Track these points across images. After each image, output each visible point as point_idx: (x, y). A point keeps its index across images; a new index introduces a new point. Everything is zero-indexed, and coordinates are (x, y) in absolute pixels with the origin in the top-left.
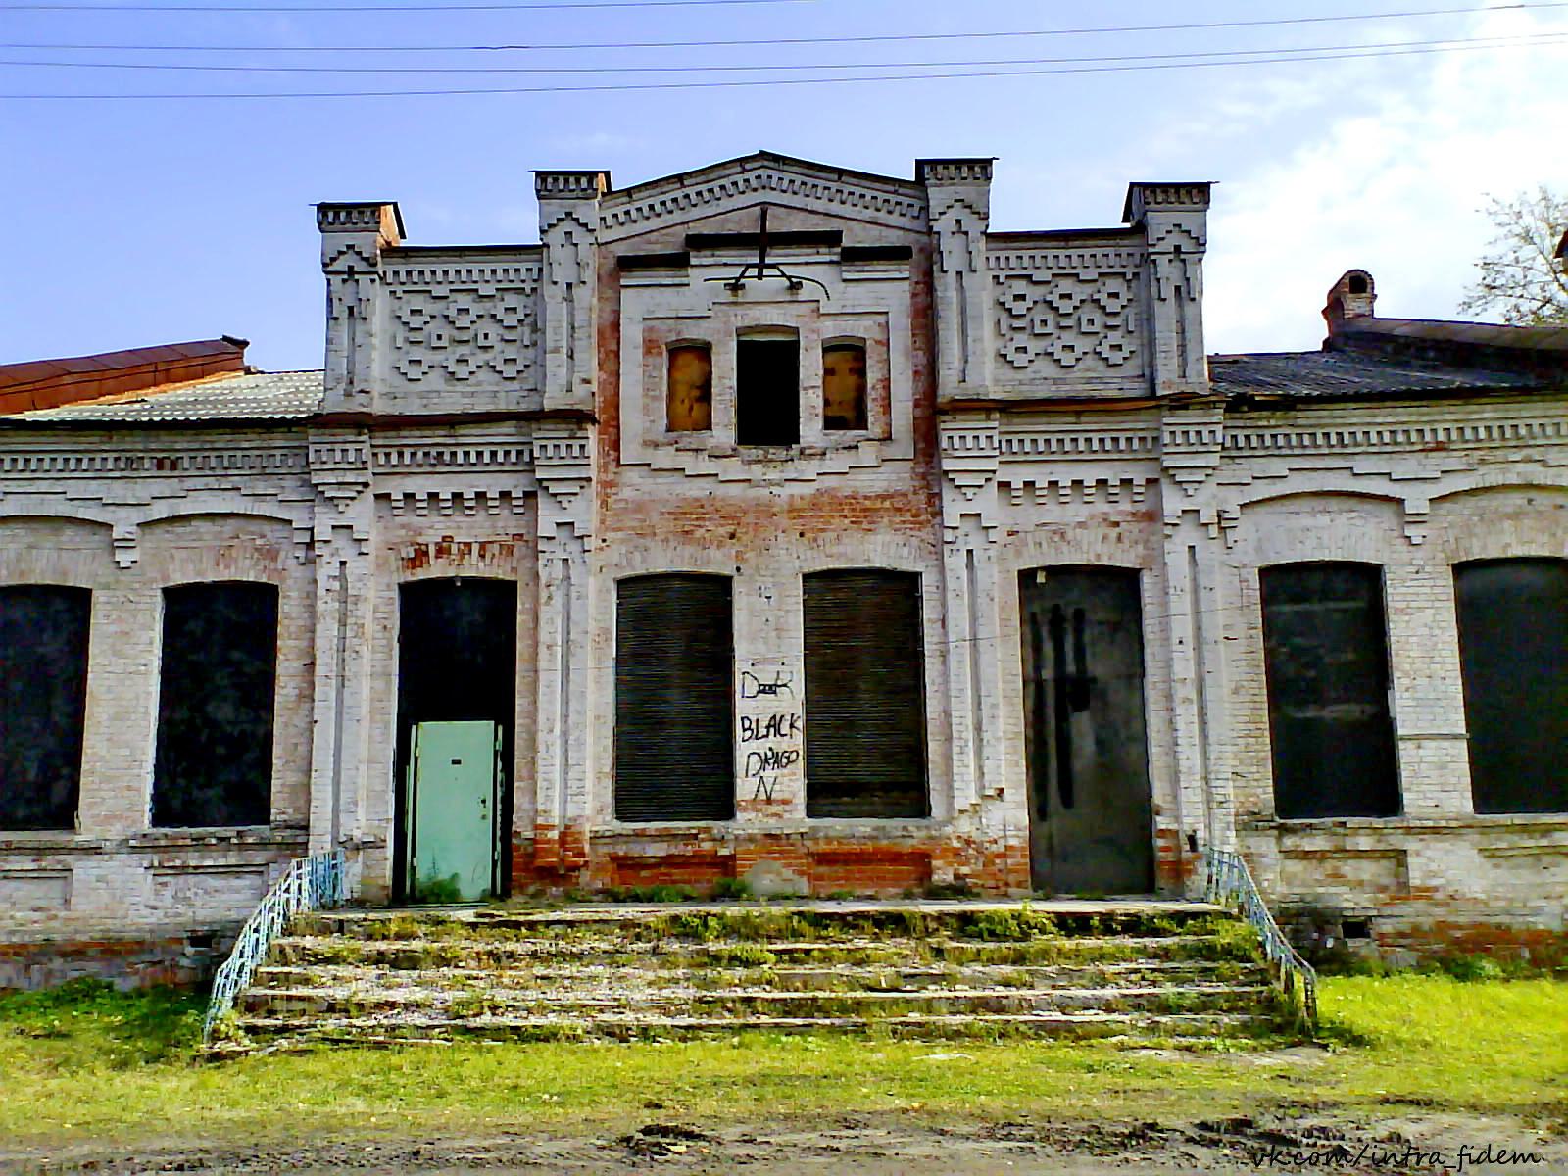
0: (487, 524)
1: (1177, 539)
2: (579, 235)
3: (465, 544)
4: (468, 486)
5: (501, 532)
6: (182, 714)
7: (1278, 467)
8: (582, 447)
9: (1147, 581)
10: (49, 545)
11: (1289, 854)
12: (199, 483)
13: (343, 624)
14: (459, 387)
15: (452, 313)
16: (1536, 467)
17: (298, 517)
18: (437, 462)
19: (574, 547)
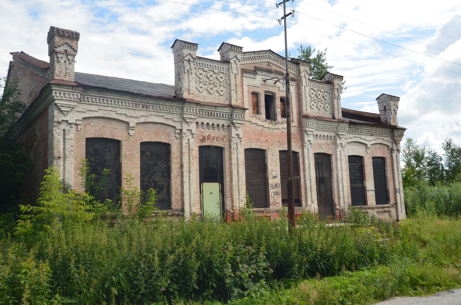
0: (218, 132)
1: (338, 149)
2: (237, 61)
3: (213, 137)
4: (216, 122)
5: (221, 134)
6: (146, 179)
7: (94, 108)
8: (244, 116)
9: (333, 158)
10: (109, 126)
12: (153, 113)
13: (189, 156)
14: (210, 96)
15: (209, 75)
16: (382, 140)
17: (178, 126)
18: (210, 115)
19: (239, 140)
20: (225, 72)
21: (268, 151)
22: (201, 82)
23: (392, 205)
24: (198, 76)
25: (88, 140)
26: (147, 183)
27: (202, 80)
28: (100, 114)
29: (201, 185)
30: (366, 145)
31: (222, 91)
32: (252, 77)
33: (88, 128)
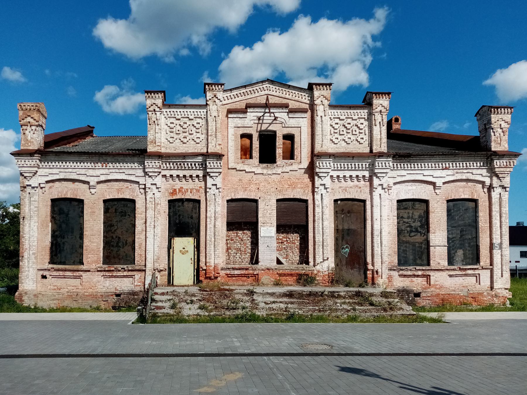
7: (404, 173)
11: (400, 276)
15: (182, 124)
20: (203, 116)
21: (259, 200)
22: (199, 132)
23: (482, 267)
24: (169, 125)
25: (53, 200)
26: (110, 239)
27: (199, 131)
28: (62, 176)
29: (172, 240)
30: (433, 184)
31: (337, 138)
32: (241, 116)
33: (53, 190)
